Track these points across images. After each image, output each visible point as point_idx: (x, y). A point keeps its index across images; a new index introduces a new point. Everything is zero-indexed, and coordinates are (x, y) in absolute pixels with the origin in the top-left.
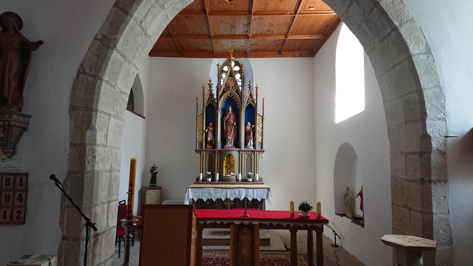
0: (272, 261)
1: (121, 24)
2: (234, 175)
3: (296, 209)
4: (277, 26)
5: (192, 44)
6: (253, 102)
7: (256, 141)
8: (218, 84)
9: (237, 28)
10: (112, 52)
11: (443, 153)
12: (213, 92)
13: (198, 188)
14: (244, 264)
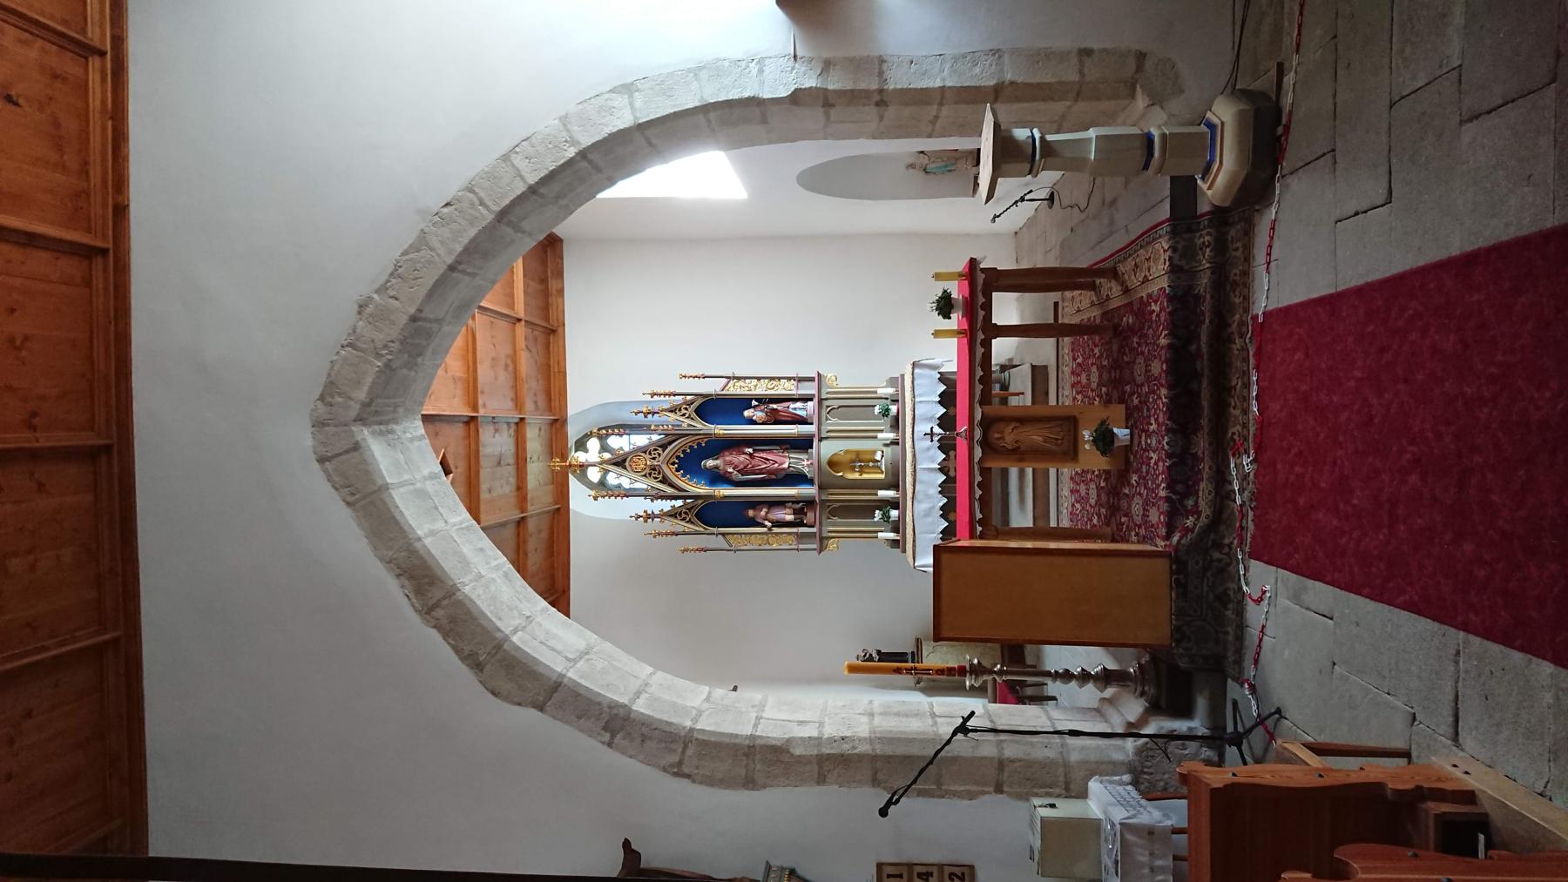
1: (580, 695)
2: (883, 452)
4: (497, 347)
5: (537, 566)
7: (794, 395)
8: (646, 497)
10: (636, 711)
11: (827, 66)
12: (665, 510)
13: (914, 541)
14: (1063, 439)
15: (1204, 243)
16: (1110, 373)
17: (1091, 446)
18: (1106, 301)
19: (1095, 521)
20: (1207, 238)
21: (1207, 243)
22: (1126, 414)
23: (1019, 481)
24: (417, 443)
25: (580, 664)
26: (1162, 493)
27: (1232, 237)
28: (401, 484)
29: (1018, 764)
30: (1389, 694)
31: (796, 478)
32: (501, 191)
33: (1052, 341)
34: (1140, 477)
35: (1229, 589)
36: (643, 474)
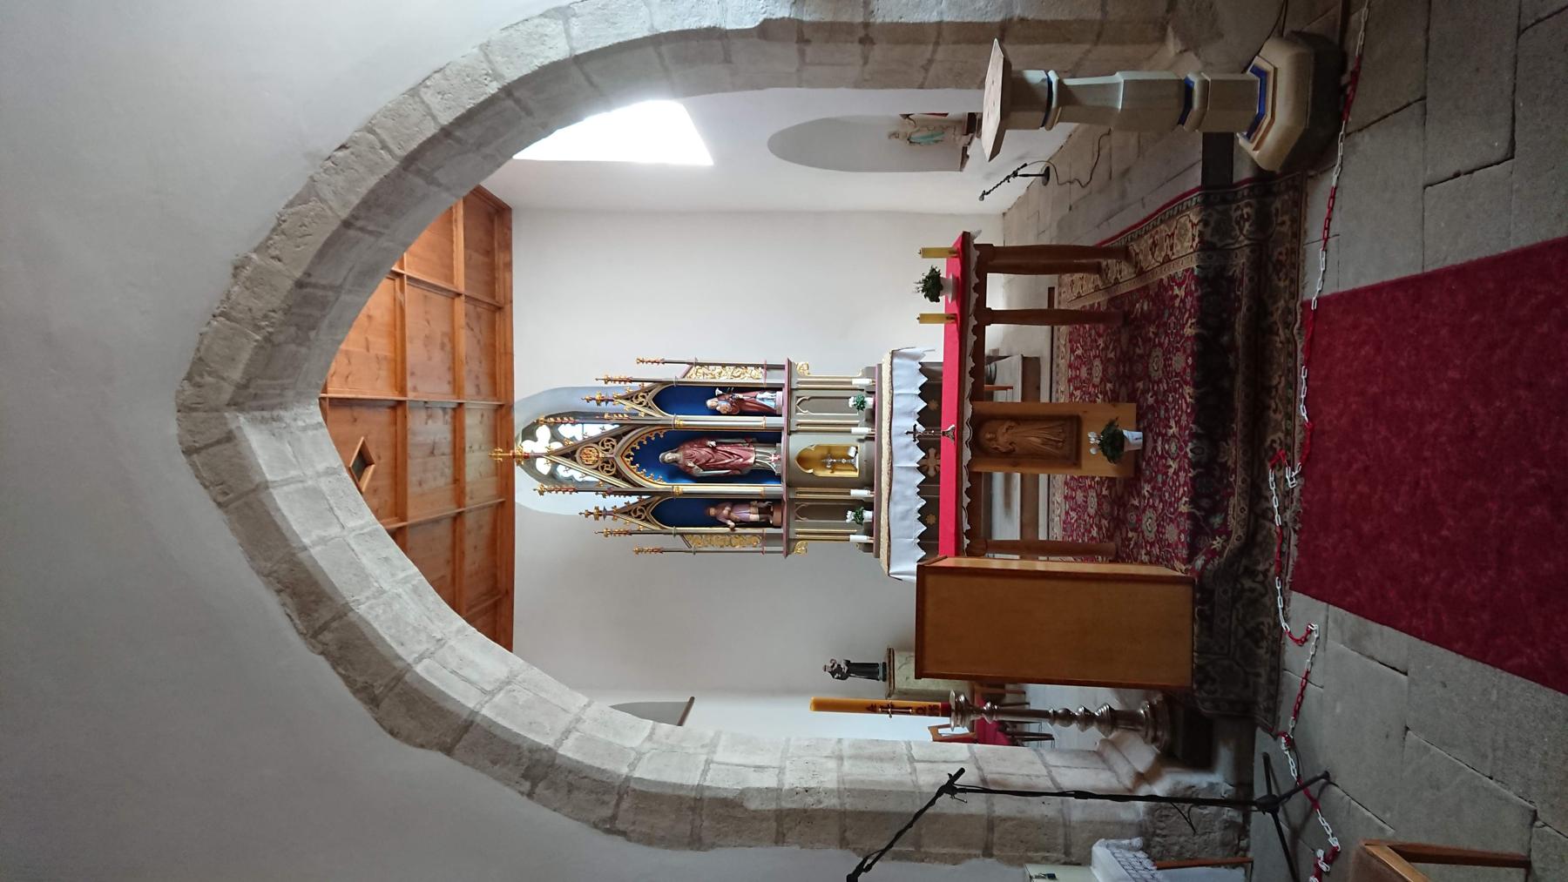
0: (1072, 358)
1: (495, 736)
2: (857, 448)
3: (939, 307)
5: (477, 565)
6: (649, 390)
7: (762, 384)
9: (437, 440)
12: (618, 507)
13: (889, 546)
15: (1242, 216)
16: (1118, 367)
17: (1097, 450)
18: (1115, 284)
19: (1094, 533)
20: (1245, 210)
21: (1246, 216)
22: (1138, 414)
23: (1004, 486)
24: (310, 433)
25: (499, 697)
26: (1184, 509)
27: (1277, 210)
28: (287, 482)
29: (1010, 823)
30: (1491, 778)
31: (761, 474)
32: (408, 132)
33: (1046, 329)
34: (1153, 488)
35: (1263, 623)
36: (595, 466)
